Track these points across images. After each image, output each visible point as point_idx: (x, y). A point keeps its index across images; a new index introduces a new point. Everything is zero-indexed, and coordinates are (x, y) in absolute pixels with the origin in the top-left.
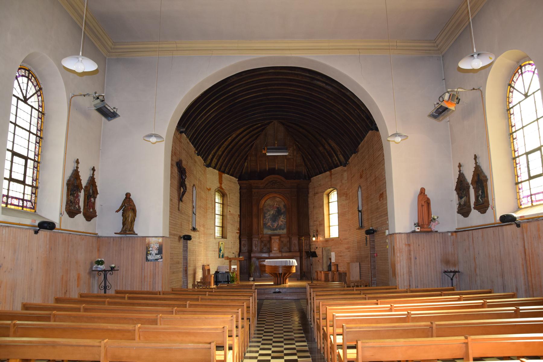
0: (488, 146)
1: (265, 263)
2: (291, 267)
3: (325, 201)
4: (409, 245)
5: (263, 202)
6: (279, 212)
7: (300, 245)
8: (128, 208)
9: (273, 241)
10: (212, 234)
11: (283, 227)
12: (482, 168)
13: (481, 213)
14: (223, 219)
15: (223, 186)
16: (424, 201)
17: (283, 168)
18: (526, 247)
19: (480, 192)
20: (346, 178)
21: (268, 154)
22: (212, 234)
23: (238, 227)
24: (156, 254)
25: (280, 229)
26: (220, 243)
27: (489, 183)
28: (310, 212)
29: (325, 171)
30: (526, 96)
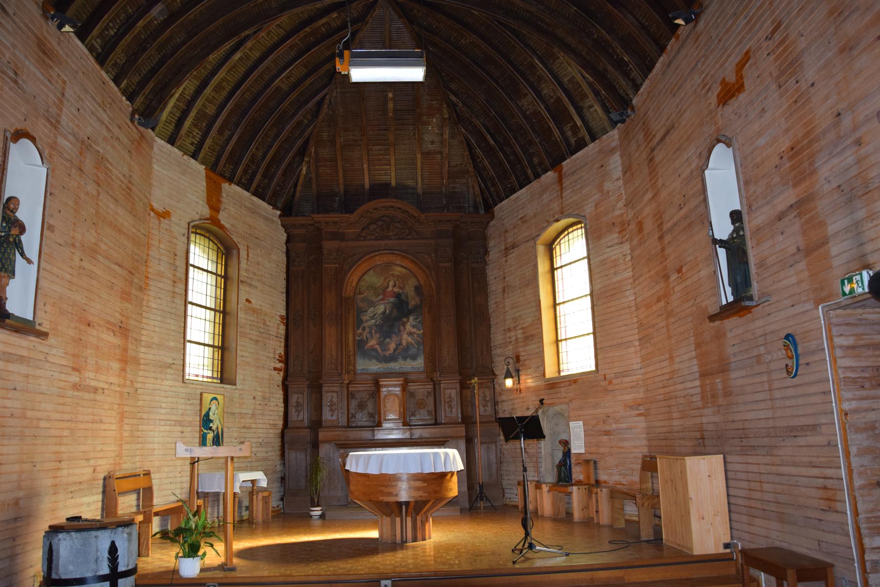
2: (441, 477)
3: (543, 267)
5: (353, 278)
6: (401, 309)
7: (466, 403)
10: (170, 366)
11: (413, 351)
14: (224, 325)
15: (223, 217)
17: (410, 183)
20: (618, 172)
21: (360, 74)
22: (170, 366)
23: (281, 350)
25: (405, 358)
26: (207, 397)
28: (492, 306)
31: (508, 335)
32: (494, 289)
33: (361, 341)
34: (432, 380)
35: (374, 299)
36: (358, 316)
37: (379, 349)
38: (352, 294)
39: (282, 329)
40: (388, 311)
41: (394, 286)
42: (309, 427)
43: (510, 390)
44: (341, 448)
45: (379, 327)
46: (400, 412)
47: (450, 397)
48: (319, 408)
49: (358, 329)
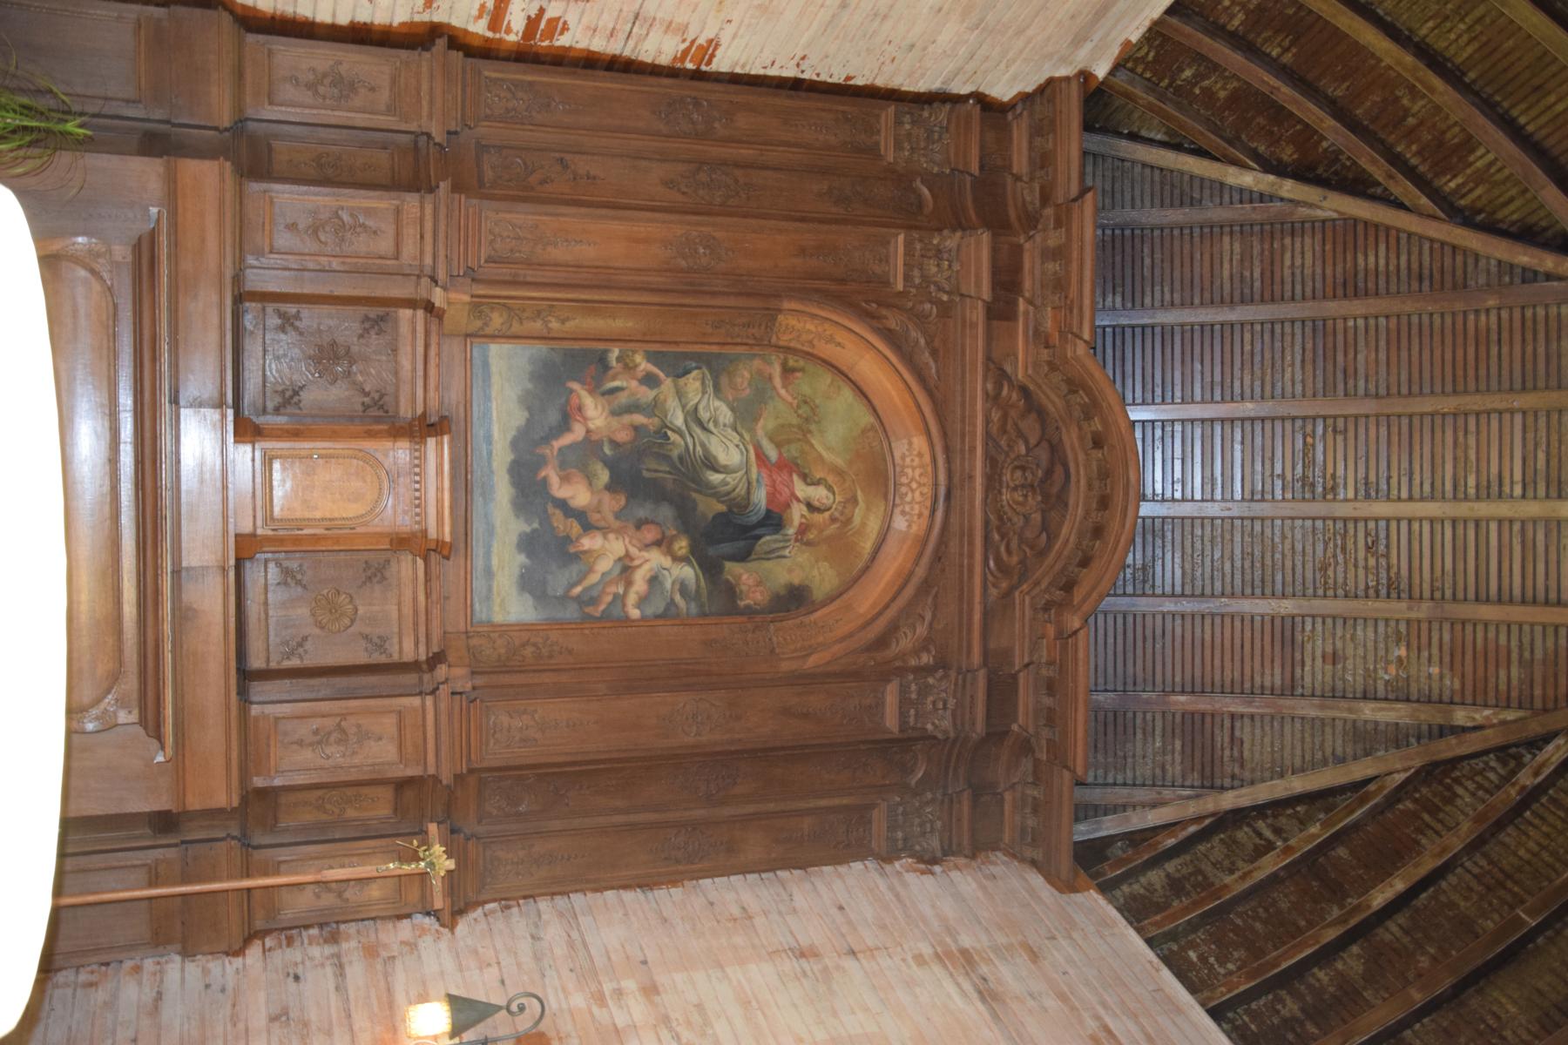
6: (729, 534)
9: (400, 453)
25: (528, 544)
31: (630, 985)
32: (800, 900)
33: (602, 361)
34: (436, 659)
35: (766, 424)
36: (704, 360)
37: (567, 439)
38: (784, 340)
39: (659, 48)
40: (715, 478)
41: (811, 507)
42: (241, 121)
44: (137, 248)
45: (653, 442)
46: (300, 523)
47: (364, 736)
48: (328, 174)
49: (652, 357)
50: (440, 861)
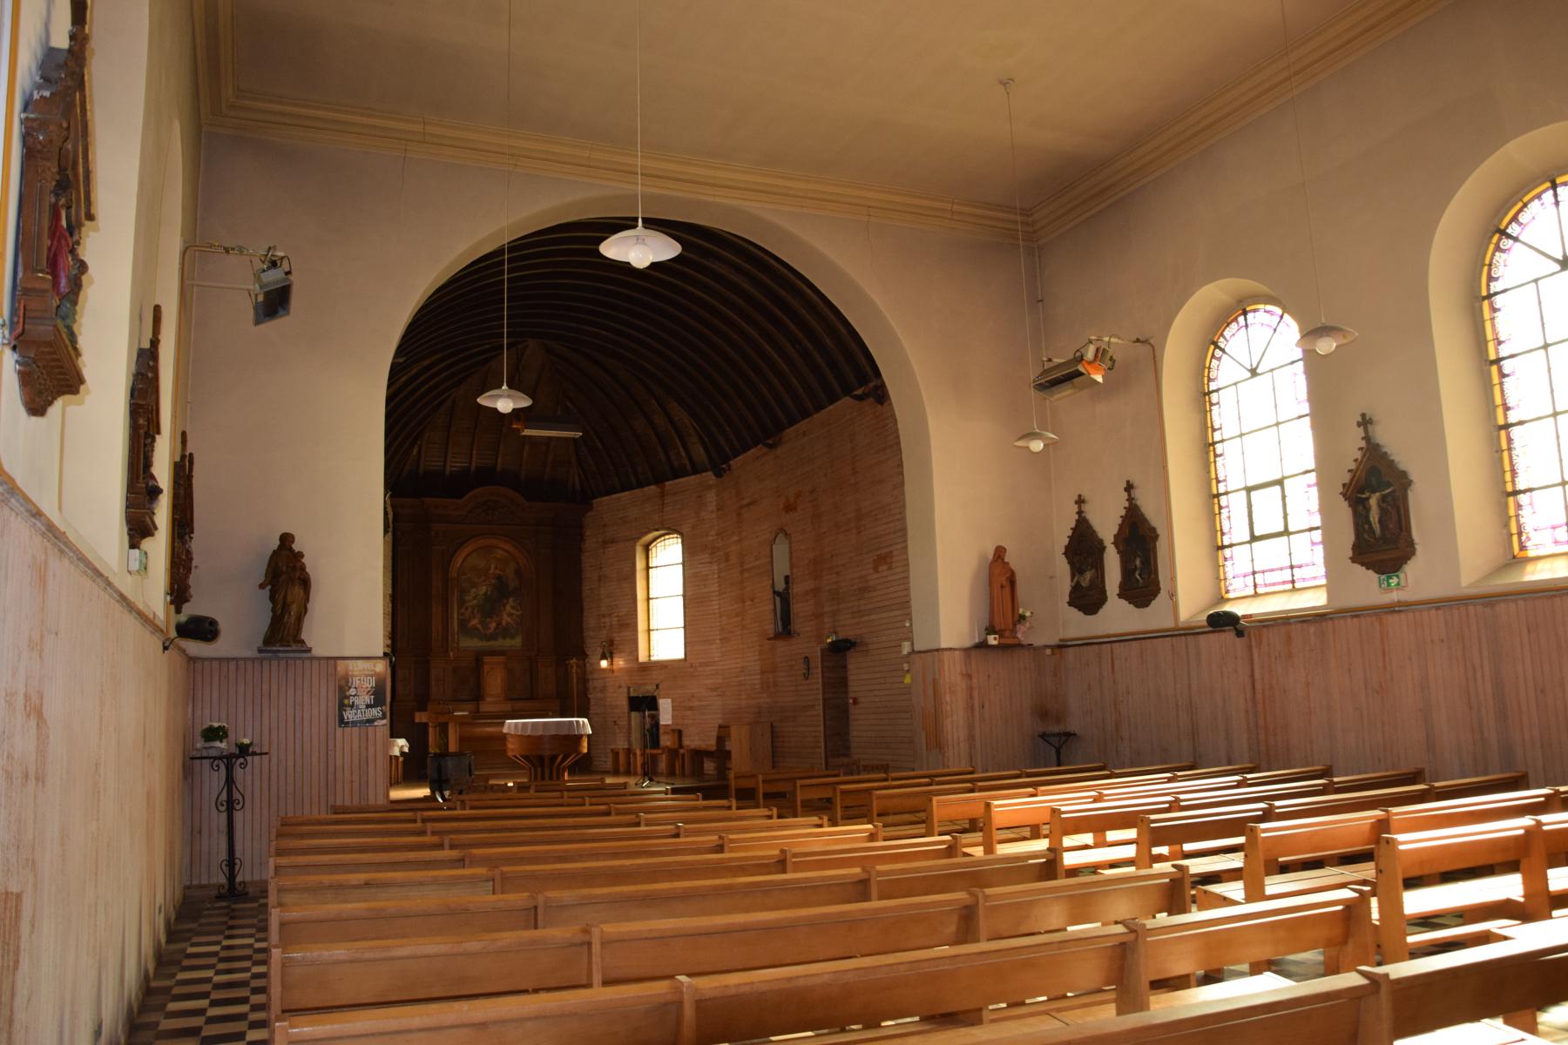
0: (1165, 467)
1: (505, 730)
3: (640, 564)
4: (970, 676)
6: (501, 590)
8: (286, 575)
12: (1144, 510)
13: (1137, 606)
16: (1000, 577)
18: (1257, 676)
19: (1138, 562)
20: (712, 506)
24: (368, 706)
27: (1161, 545)
29: (640, 485)
30: (1254, 372)
43: (604, 670)
50: (573, 661)
